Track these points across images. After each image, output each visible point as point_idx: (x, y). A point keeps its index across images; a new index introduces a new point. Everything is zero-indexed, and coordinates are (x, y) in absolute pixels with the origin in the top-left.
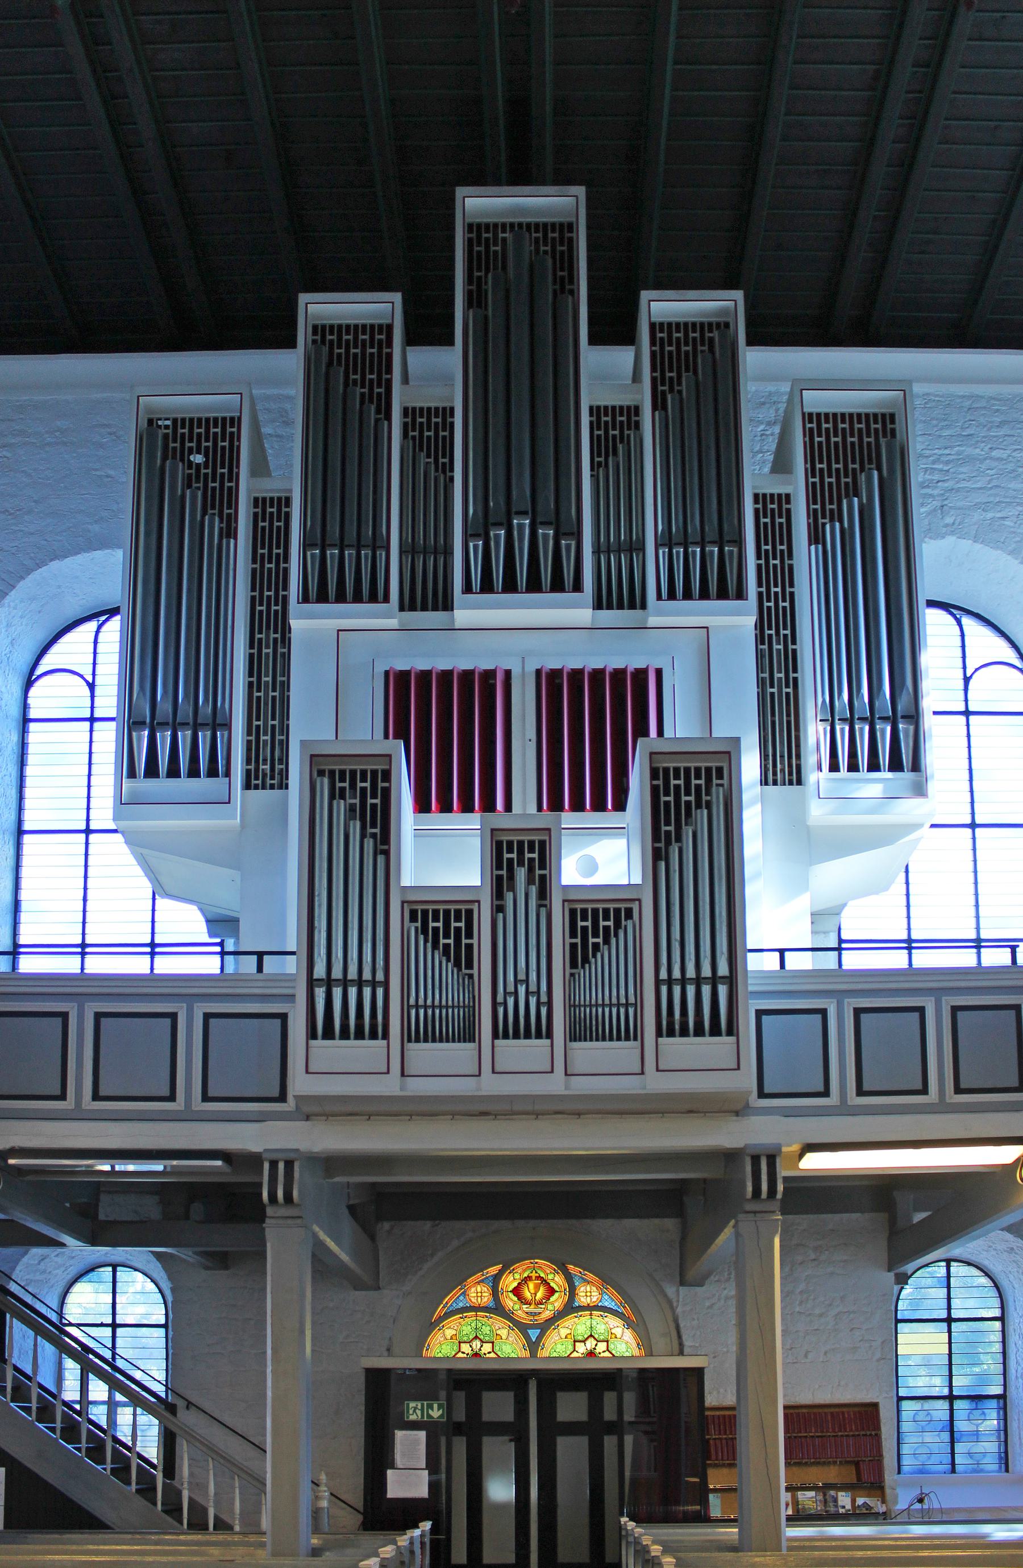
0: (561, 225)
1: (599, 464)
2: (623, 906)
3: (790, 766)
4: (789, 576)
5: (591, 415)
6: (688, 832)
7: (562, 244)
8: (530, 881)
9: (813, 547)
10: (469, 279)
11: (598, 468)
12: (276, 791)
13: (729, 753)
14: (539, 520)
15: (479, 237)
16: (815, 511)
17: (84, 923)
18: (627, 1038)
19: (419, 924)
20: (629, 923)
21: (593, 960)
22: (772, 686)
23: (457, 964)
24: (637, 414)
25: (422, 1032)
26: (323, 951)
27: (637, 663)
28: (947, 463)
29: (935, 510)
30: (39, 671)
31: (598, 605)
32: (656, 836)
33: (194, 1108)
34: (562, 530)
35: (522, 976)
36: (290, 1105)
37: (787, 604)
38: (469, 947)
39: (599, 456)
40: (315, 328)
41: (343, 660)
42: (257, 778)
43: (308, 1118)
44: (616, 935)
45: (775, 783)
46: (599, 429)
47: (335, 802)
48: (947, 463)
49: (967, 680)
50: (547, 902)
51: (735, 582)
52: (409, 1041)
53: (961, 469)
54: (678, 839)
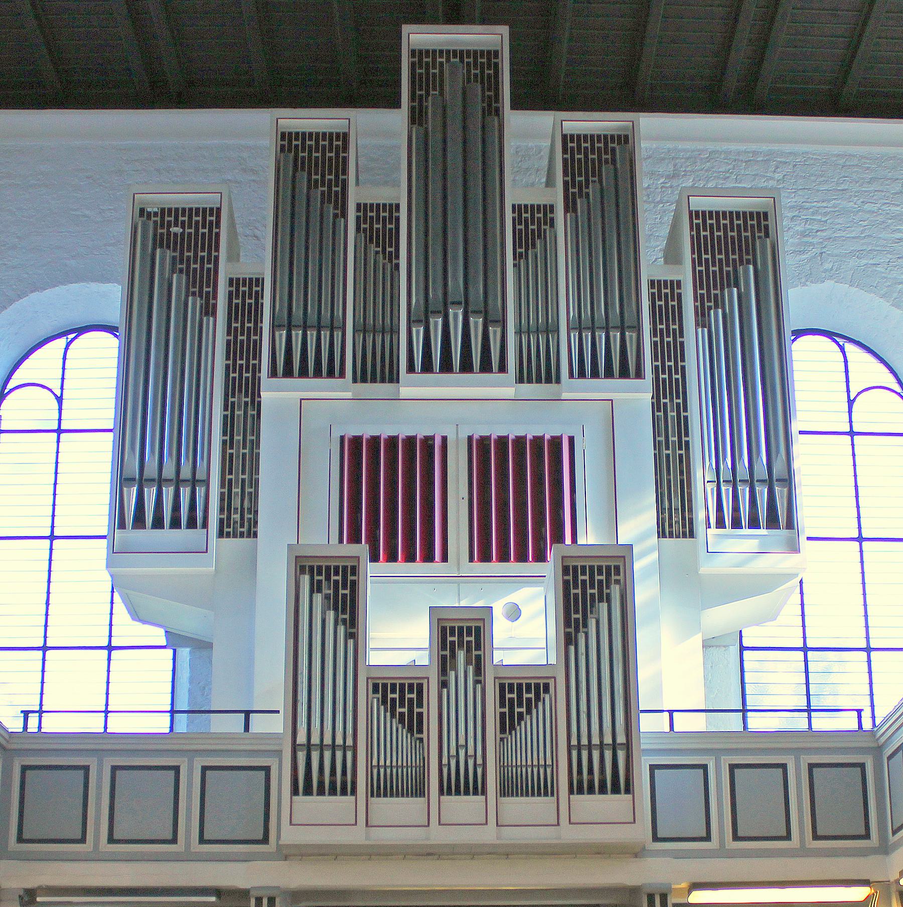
0: (489, 52)
1: (521, 254)
2: (541, 682)
3: (684, 518)
4: (680, 352)
5: (514, 212)
6: (592, 623)
7: (489, 68)
8: (468, 662)
9: (700, 330)
10: (413, 97)
11: (520, 259)
12: (245, 539)
13: (624, 557)
14: (470, 309)
15: (420, 61)
16: (702, 295)
17: (46, 626)
18: (546, 794)
19: (380, 696)
20: (547, 697)
21: (518, 728)
22: (667, 449)
23: (410, 730)
24: (552, 211)
25: (383, 788)
26: (305, 719)
27: (548, 432)
28: (826, 214)
29: (814, 257)
30: (10, 386)
31: (520, 380)
32: (567, 622)
33: (193, 850)
34: (490, 318)
35: (462, 741)
36: (271, 847)
37: (679, 376)
38: (420, 715)
39: (521, 247)
40: (283, 135)
41: (308, 421)
42: (229, 526)
43: (286, 858)
44: (536, 707)
45: (671, 536)
46: (520, 224)
47: (314, 595)
48: (826, 214)
49: (851, 403)
50: (482, 678)
51: (634, 359)
52: (372, 796)
53: (840, 221)
54: (585, 625)
